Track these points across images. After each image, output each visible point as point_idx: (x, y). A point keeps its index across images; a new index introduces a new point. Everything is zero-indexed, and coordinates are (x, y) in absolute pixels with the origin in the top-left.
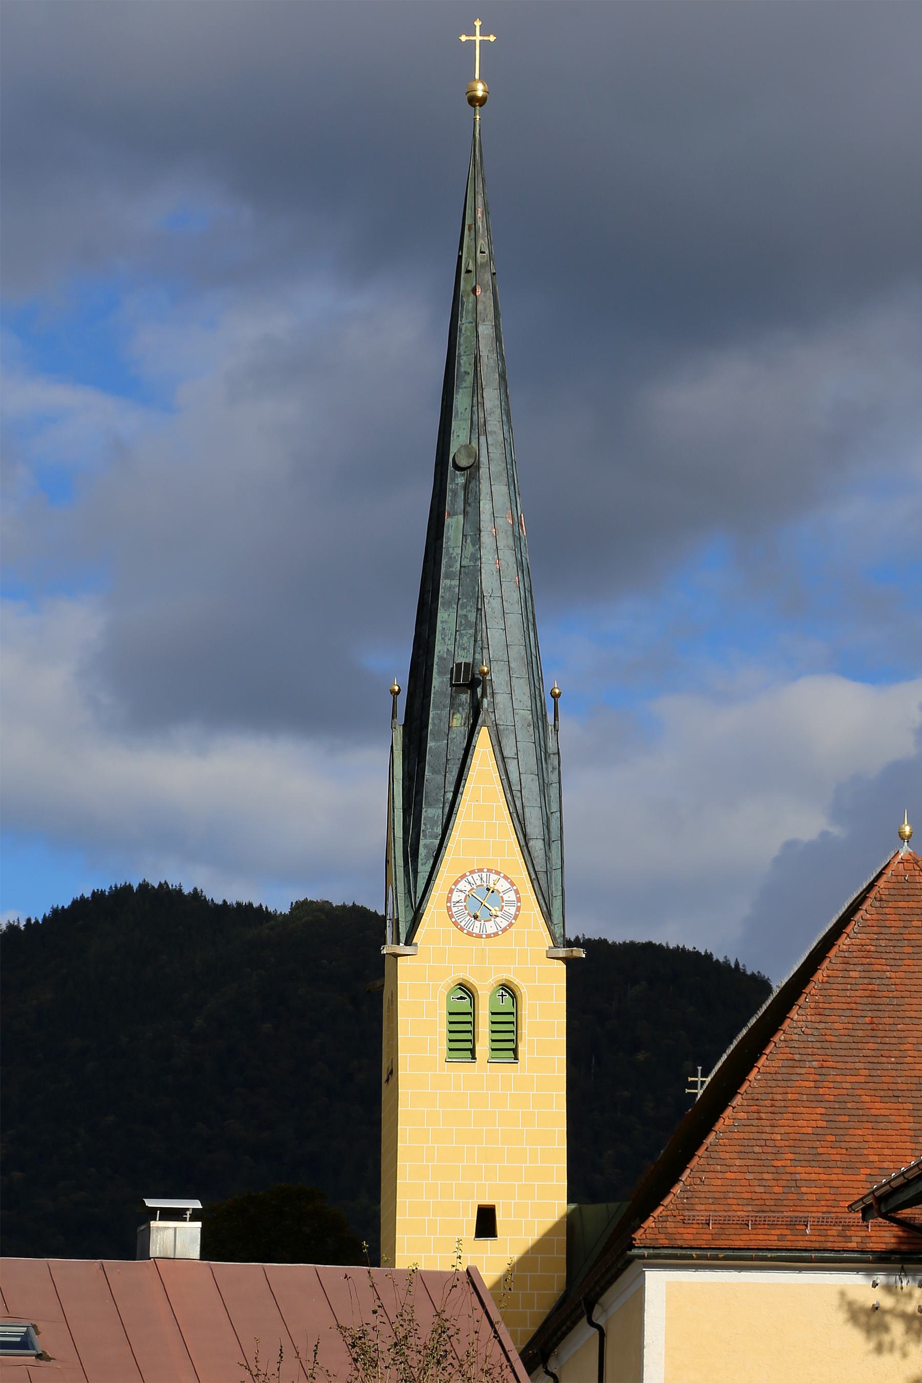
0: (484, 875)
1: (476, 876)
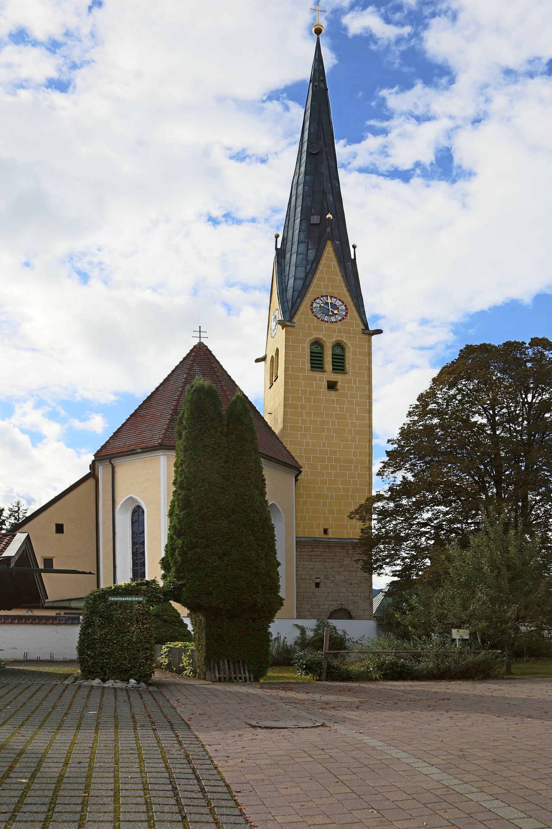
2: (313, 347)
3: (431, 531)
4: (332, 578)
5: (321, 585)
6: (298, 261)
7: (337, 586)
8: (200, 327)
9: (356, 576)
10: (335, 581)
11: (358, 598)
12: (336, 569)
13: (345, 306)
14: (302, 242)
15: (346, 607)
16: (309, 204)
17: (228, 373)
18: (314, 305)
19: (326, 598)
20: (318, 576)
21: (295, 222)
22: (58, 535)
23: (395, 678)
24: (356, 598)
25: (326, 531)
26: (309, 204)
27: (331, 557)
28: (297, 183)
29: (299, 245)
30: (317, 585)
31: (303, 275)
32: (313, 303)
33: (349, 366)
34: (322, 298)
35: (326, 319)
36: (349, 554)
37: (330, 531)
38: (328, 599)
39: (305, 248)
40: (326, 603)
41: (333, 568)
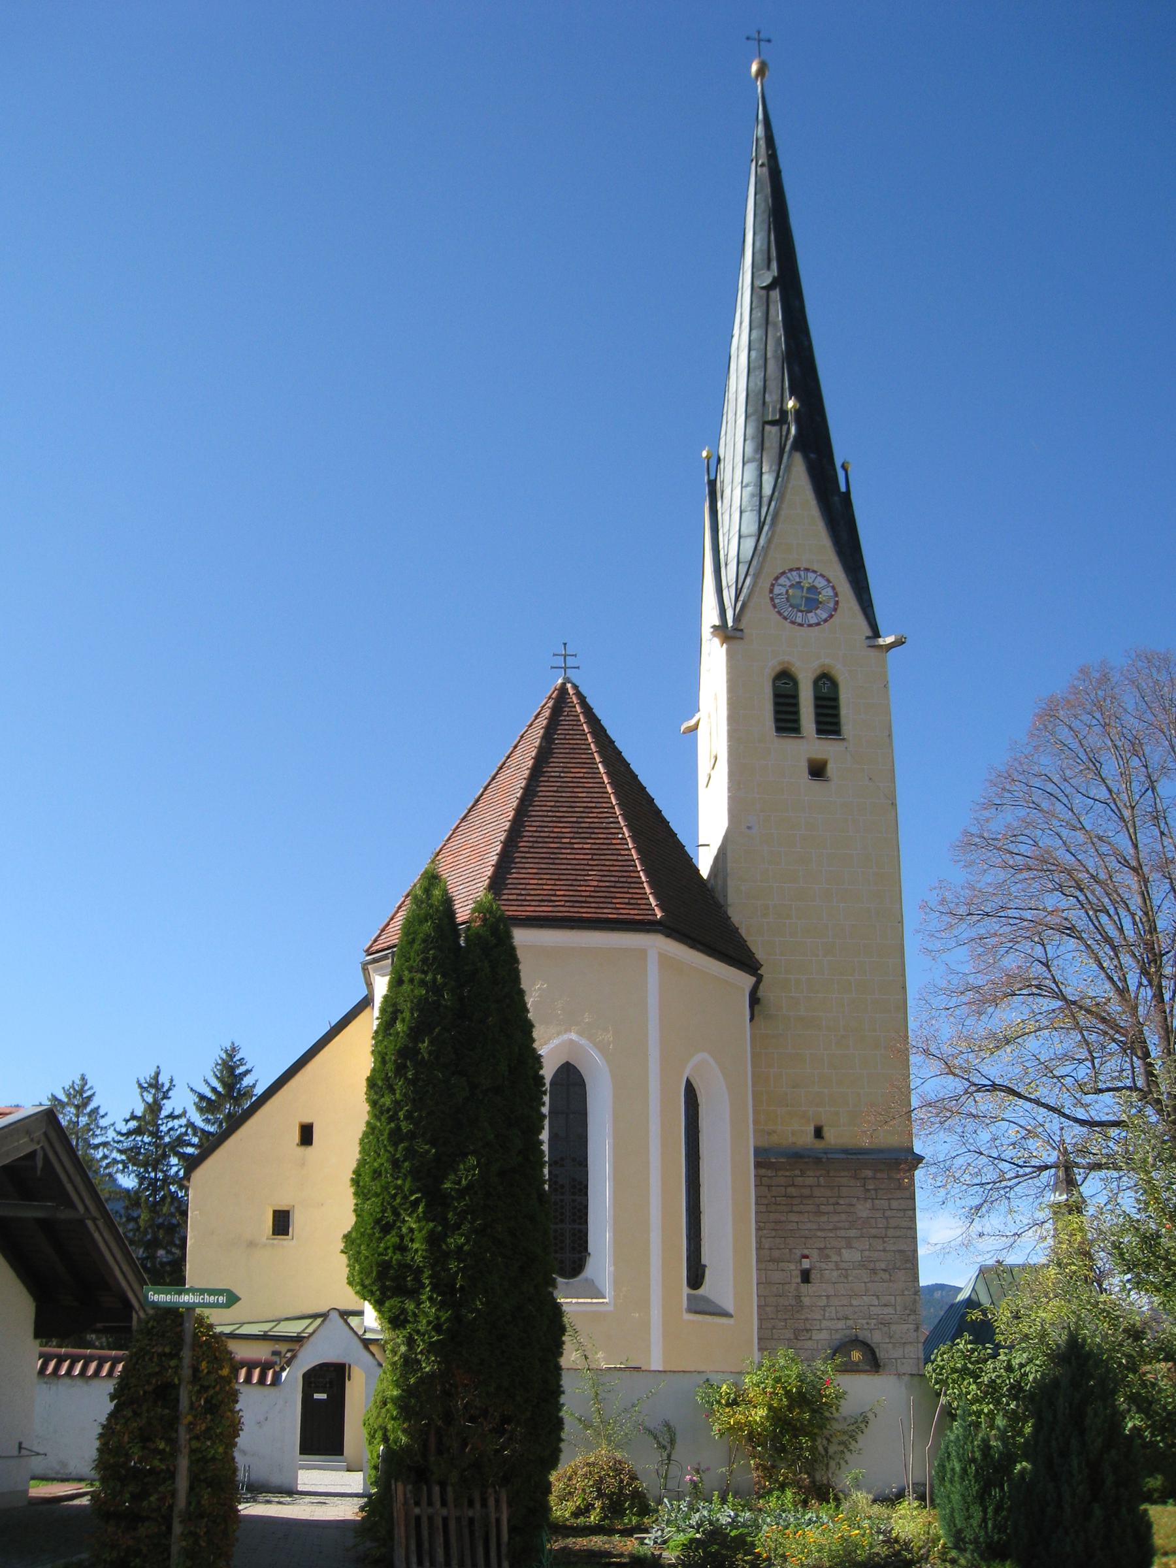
0: (802, 573)
1: (794, 573)
2: (779, 683)
3: (1127, 1285)
4: (835, 1258)
5: (814, 1275)
6: (745, 499)
7: (846, 1277)
8: (575, 656)
9: (884, 1251)
10: (843, 1265)
11: (890, 1310)
12: (842, 1233)
13: (833, 588)
14: (750, 461)
15: (862, 1335)
16: (759, 383)
17: (608, 732)
18: (777, 590)
19: (824, 1310)
20: (806, 1252)
21: (738, 423)
22: (302, 1149)
23: (325, 1368)
24: (886, 1310)
25: (819, 1133)
26: (759, 383)
27: (832, 1201)
28: (738, 348)
29: (746, 467)
30: (806, 1276)
31: (754, 528)
32: (773, 585)
33: (847, 727)
34: (789, 575)
35: (799, 620)
36: (868, 1190)
37: (828, 1133)
38: (827, 1315)
39: (757, 473)
40: (825, 1324)
41: (836, 1229)
